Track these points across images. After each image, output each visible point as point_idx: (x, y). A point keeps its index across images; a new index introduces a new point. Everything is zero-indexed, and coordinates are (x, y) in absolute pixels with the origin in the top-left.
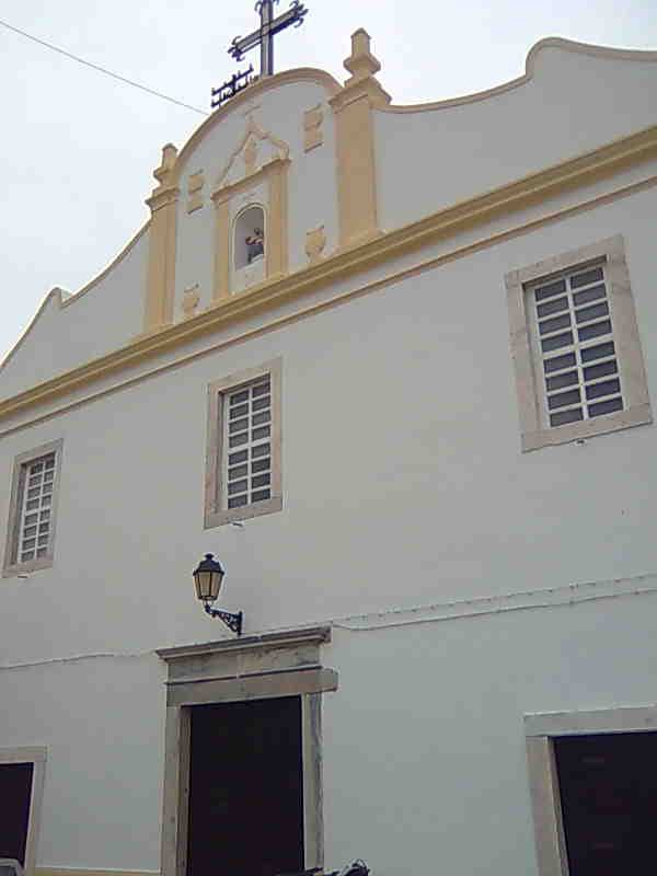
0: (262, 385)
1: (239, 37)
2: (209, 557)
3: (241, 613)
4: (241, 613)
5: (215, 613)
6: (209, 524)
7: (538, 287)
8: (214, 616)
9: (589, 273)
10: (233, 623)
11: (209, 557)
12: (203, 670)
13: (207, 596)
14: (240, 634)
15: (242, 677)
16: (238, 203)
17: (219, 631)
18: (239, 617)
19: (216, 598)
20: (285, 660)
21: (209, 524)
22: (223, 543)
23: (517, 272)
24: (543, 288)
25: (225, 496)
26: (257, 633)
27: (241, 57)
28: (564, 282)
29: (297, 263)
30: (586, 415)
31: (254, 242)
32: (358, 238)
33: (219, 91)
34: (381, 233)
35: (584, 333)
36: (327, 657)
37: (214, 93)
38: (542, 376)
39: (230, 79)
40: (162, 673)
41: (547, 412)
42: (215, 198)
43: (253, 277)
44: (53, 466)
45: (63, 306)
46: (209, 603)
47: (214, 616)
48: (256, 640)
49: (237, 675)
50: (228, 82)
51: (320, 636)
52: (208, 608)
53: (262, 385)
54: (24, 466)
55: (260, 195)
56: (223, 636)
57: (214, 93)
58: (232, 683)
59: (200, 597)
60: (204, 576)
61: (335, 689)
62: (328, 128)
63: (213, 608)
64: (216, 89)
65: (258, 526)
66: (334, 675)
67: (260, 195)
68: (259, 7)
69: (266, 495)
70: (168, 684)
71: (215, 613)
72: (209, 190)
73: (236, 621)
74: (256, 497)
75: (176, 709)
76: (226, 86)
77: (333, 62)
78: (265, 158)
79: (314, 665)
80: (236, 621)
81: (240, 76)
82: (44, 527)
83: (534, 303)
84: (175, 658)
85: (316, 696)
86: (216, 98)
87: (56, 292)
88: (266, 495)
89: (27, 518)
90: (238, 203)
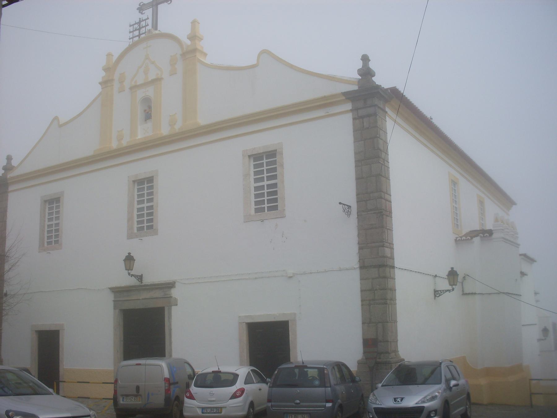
0: (150, 180)
2: (129, 253)
5: (132, 275)
10: (139, 278)
11: (129, 253)
14: (142, 283)
15: (143, 299)
16: (140, 94)
17: (133, 281)
19: (132, 270)
20: (158, 294)
24: (256, 157)
27: (144, 12)
28: (263, 156)
29: (165, 131)
30: (53, 243)
31: (148, 113)
33: (133, 25)
35: (269, 178)
37: (130, 26)
38: (253, 192)
39: (138, 21)
40: (110, 297)
41: (253, 206)
42: (131, 88)
44: (60, 203)
45: (61, 126)
46: (130, 271)
48: (148, 285)
50: (137, 22)
51: (171, 285)
52: (129, 274)
53: (150, 180)
54: (45, 201)
55: (150, 92)
57: (130, 26)
63: (131, 274)
64: (131, 24)
66: (176, 300)
67: (150, 92)
69: (57, 242)
71: (132, 275)
74: (270, 209)
76: (136, 24)
77: (183, 34)
78: (152, 76)
79: (169, 296)
81: (143, 21)
83: (252, 163)
84: (118, 291)
86: (131, 36)
87: (56, 118)
88: (275, 208)
89: (48, 226)
90: (140, 94)
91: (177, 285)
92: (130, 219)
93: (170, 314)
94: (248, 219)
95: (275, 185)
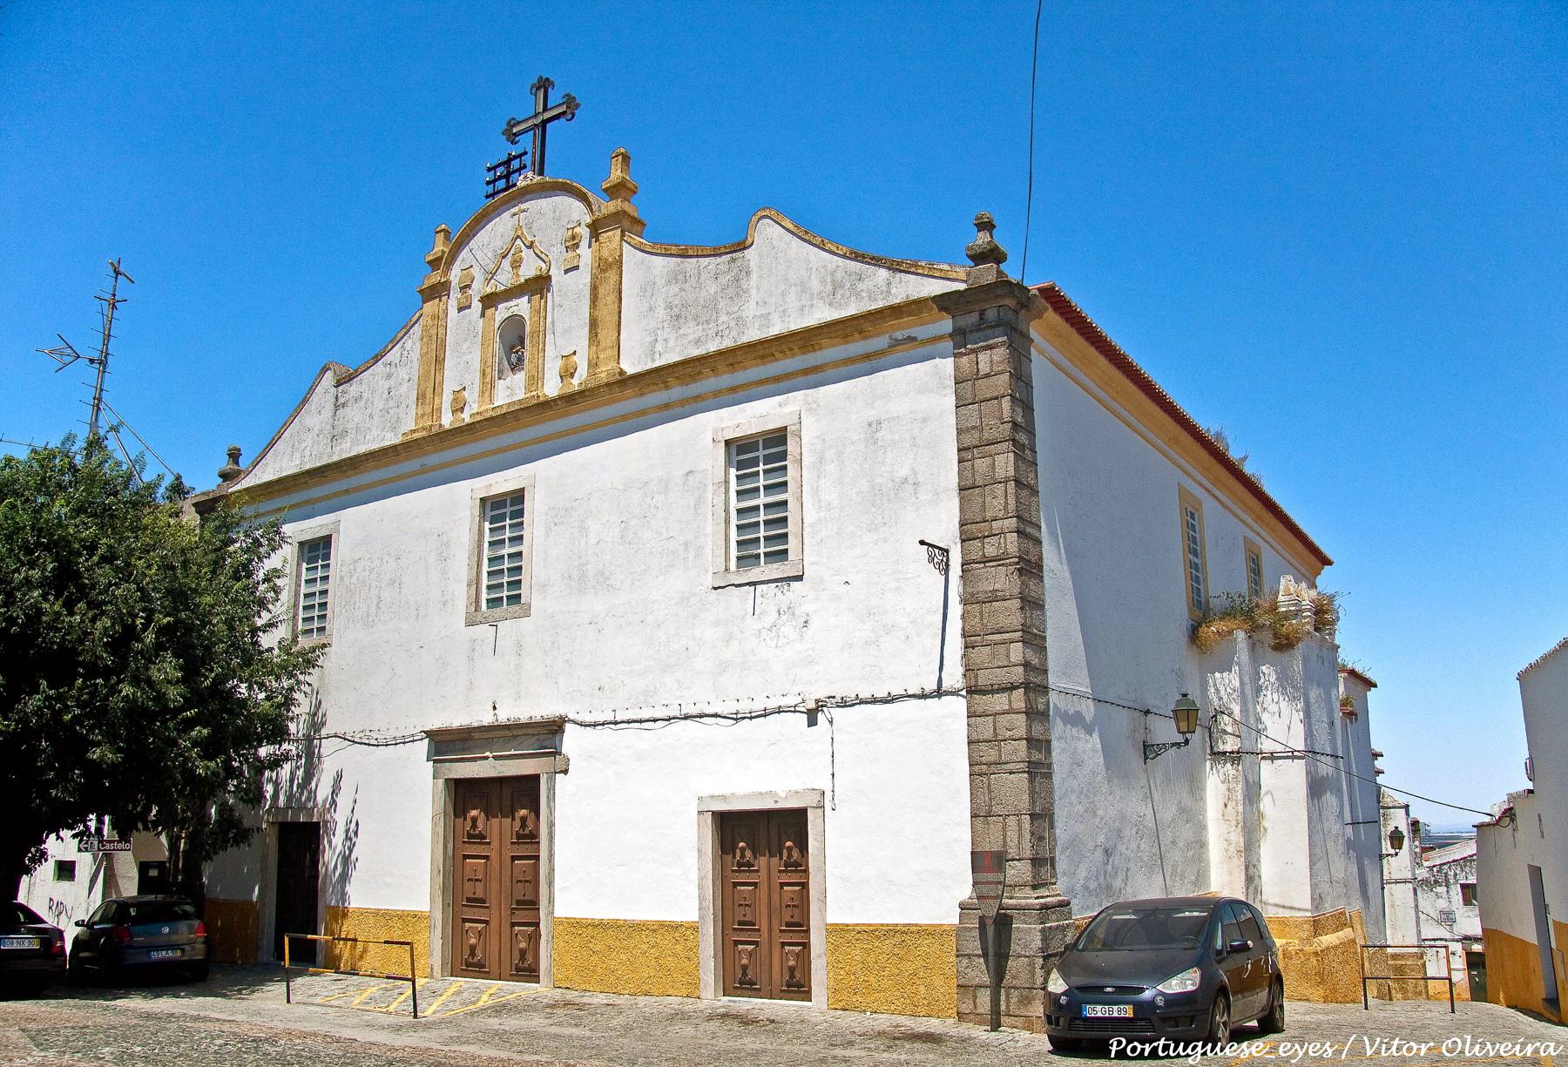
1: (513, 119)
6: (470, 623)
8: (817, 701)
9: (777, 439)
12: (464, 750)
21: (470, 623)
24: (741, 450)
25: (484, 596)
29: (552, 388)
34: (622, 372)
39: (505, 158)
43: (511, 391)
47: (817, 701)
51: (553, 728)
62: (586, 253)
67: (522, 306)
68: (534, 90)
69: (515, 599)
72: (479, 288)
75: (441, 782)
78: (529, 269)
82: (323, 605)
87: (565, 772)
90: (502, 311)
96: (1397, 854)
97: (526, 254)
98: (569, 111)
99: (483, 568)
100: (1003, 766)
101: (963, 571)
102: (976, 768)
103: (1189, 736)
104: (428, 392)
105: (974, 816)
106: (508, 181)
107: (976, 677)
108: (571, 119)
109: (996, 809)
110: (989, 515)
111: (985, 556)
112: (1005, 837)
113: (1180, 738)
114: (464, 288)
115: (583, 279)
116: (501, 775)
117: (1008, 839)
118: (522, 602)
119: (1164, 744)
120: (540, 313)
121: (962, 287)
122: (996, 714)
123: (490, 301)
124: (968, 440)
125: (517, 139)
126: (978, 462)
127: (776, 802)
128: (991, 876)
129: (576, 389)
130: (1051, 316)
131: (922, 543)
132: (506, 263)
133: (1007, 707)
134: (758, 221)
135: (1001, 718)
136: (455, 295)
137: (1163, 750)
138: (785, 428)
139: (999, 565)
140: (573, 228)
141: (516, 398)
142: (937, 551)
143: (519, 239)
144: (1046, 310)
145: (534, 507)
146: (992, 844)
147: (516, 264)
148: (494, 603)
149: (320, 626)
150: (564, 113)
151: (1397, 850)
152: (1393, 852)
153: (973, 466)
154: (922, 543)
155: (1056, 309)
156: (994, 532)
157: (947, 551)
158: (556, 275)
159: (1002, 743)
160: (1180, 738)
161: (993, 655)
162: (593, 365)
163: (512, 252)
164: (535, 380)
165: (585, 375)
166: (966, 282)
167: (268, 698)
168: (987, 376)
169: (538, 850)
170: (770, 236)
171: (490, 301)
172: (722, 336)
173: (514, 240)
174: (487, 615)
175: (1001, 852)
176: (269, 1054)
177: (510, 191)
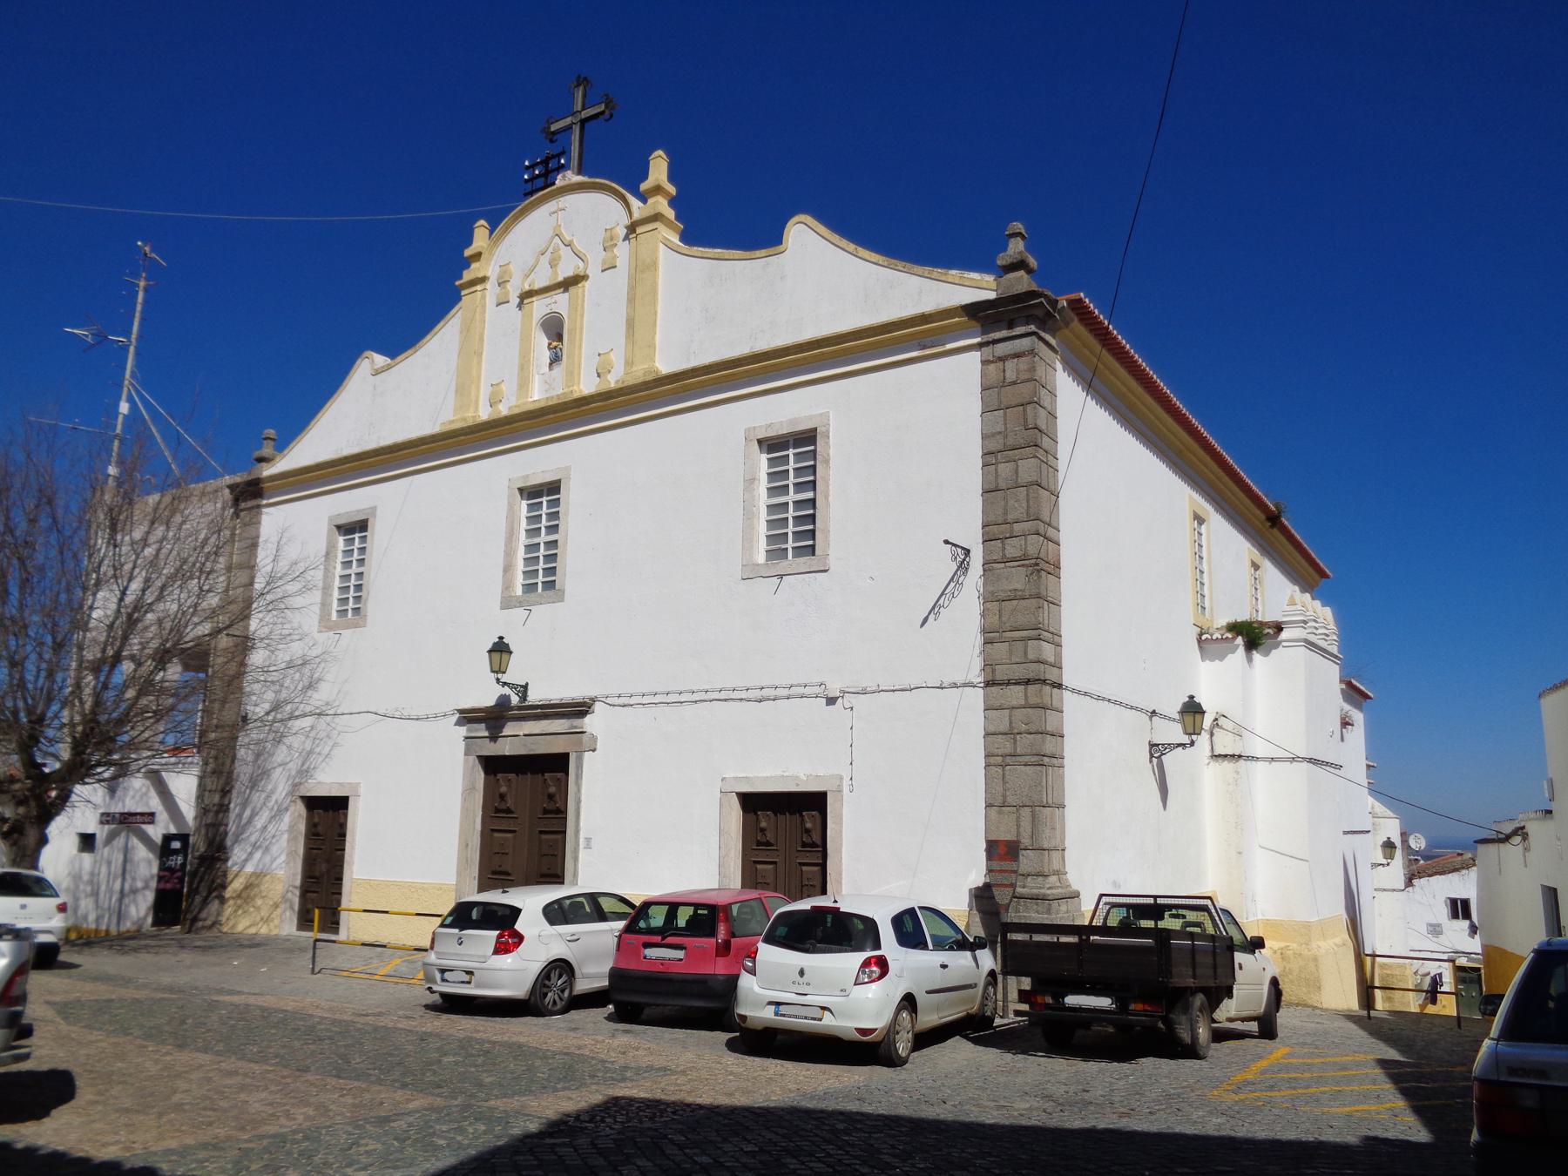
0: (553, 488)
2: (501, 638)
3: (527, 684)
4: (527, 684)
7: (769, 443)
9: (807, 438)
10: (519, 691)
11: (501, 638)
13: (498, 669)
15: (525, 735)
18: (525, 687)
22: (512, 626)
23: (754, 427)
24: (773, 444)
26: (751, 481)
29: (587, 386)
32: (639, 374)
35: (799, 487)
36: (589, 723)
46: (500, 676)
49: (521, 733)
51: (580, 709)
52: (498, 680)
53: (553, 488)
56: (588, 840)
58: (518, 739)
59: (493, 672)
60: (496, 656)
61: (594, 750)
65: (544, 612)
66: (594, 739)
69: (550, 585)
70: (467, 738)
73: (523, 690)
74: (799, 552)
80: (523, 690)
85: (580, 753)
91: (598, 706)
92: (508, 568)
93: (580, 766)
94: (751, 574)
95: (812, 502)
96: (1388, 864)
97: (565, 252)
98: (607, 113)
99: (519, 555)
100: (1018, 759)
101: (984, 570)
102: (992, 760)
103: (1194, 737)
104: (464, 388)
105: (988, 806)
106: (547, 166)
107: (993, 671)
108: (609, 119)
109: (1011, 800)
110: (1010, 517)
111: (1004, 555)
112: (1018, 826)
113: (1186, 739)
114: (502, 283)
115: (620, 277)
116: (532, 753)
117: (1022, 829)
118: (557, 587)
119: (1169, 745)
120: (575, 307)
121: (992, 295)
122: (1013, 708)
123: (527, 295)
124: (993, 446)
125: (555, 138)
126: (1001, 466)
127: (797, 785)
128: (1006, 865)
129: (612, 385)
130: (1076, 325)
131: (946, 542)
132: (545, 260)
133: (1023, 703)
134: (797, 223)
135: (1017, 713)
136: (491, 286)
137: (1167, 750)
138: (816, 429)
139: (1019, 566)
140: (611, 229)
141: (554, 393)
142: (959, 550)
143: (557, 237)
144: (1072, 320)
145: (571, 497)
146: (1006, 835)
147: (553, 264)
148: (530, 588)
149: (362, 546)
150: (602, 113)
151: (1389, 861)
152: (1384, 862)
153: (996, 470)
154: (946, 542)
155: (1081, 320)
156: (1015, 534)
157: (968, 551)
158: (593, 271)
159: (1018, 737)
160: (1186, 739)
161: (1011, 651)
162: (629, 363)
163: (550, 250)
164: (571, 376)
165: (622, 372)
166: (996, 290)
167: (251, 1051)
168: (1014, 383)
169: (565, 825)
170: (803, 235)
171: (527, 295)
172: (756, 339)
173: (553, 238)
174: (522, 600)
175: (1014, 842)
176: (299, 1029)
177: (514, 425)
